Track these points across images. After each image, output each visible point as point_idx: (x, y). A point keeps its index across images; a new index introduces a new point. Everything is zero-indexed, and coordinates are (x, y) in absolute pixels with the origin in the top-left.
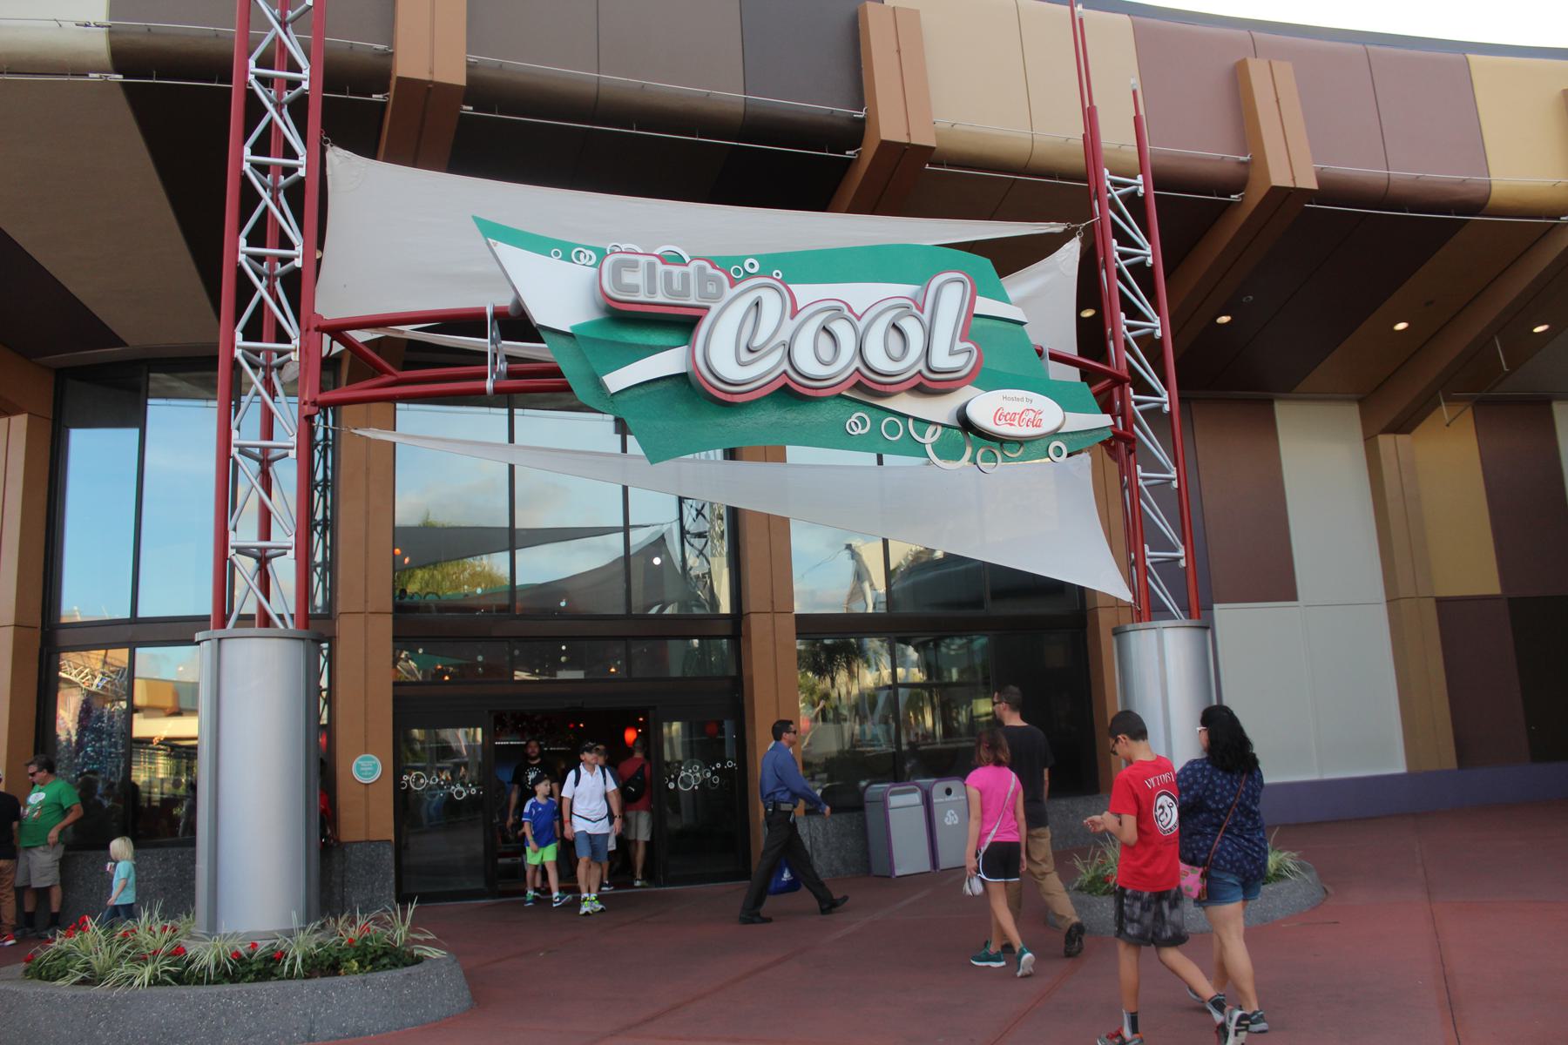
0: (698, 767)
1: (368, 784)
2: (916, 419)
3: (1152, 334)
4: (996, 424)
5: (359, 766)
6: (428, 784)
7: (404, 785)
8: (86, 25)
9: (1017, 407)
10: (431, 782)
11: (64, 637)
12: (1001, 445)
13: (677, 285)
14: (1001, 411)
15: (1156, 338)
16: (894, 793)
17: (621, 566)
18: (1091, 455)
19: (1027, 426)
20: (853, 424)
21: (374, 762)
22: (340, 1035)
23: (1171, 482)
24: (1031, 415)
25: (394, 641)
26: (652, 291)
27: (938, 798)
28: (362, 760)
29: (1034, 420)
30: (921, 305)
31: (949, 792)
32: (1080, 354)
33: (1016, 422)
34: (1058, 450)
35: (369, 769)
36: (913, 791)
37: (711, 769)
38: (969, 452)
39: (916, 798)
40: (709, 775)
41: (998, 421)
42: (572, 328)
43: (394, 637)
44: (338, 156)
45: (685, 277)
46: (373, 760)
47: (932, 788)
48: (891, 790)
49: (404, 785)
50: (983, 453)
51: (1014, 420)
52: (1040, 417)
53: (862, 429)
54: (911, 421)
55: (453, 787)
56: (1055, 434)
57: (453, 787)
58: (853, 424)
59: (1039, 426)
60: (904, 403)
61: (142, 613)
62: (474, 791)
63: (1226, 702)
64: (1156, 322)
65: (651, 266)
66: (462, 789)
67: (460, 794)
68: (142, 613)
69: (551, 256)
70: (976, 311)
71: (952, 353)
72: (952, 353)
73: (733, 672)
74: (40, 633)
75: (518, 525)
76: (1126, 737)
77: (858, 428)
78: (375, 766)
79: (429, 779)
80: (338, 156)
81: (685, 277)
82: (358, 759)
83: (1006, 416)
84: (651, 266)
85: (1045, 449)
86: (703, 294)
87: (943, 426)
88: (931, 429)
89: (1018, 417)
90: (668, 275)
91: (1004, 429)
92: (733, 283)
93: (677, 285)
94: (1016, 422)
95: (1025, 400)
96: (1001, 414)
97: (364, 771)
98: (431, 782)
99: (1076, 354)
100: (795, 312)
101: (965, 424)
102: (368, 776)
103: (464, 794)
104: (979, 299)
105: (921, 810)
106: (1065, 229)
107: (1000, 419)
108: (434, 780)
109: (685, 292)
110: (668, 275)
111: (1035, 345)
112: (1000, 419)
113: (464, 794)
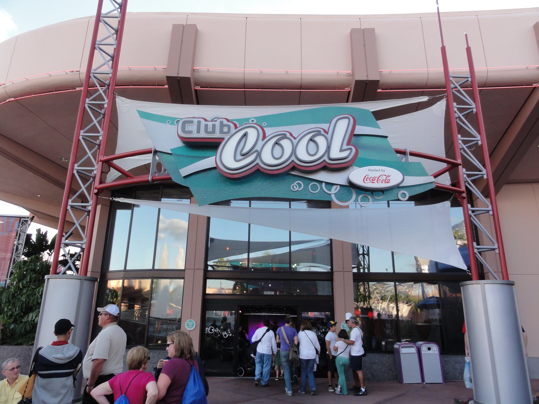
0: (315, 330)
1: (190, 331)
2: (327, 183)
3: (477, 143)
4: (364, 183)
5: (188, 324)
6: (215, 331)
7: (206, 331)
8: (73, 72)
9: (377, 174)
10: (216, 331)
11: (109, 275)
12: (372, 193)
13: (210, 129)
14: (367, 176)
15: (479, 145)
16: (403, 347)
17: (250, 251)
18: (451, 202)
19: (382, 183)
20: (295, 186)
21: (193, 323)
22: (452, 376)
23: (489, 212)
24: (384, 177)
25: (354, 282)
26: (198, 132)
27: (424, 349)
28: (189, 322)
29: (386, 180)
30: (327, 131)
31: (429, 349)
32: (447, 157)
33: (376, 181)
34: (404, 195)
35: (192, 325)
36: (413, 347)
37: (320, 331)
38: (354, 196)
39: (413, 350)
40: (319, 334)
41: (365, 180)
42: (171, 150)
43: (354, 280)
44: (120, 100)
45: (214, 126)
46: (193, 322)
47: (421, 347)
48: (401, 346)
49: (206, 331)
50: (362, 197)
51: (374, 180)
52: (389, 178)
53: (299, 188)
54: (324, 184)
55: (223, 333)
56: (398, 187)
57: (223, 333)
58: (295, 186)
59: (389, 183)
60: (323, 176)
61: (128, 268)
62: (231, 335)
63: (304, 332)
64: (478, 137)
65: (199, 123)
66: (226, 334)
67: (225, 335)
68: (128, 268)
69: (166, 123)
70: (356, 133)
71: (341, 150)
72: (341, 150)
73: (331, 294)
74: (100, 274)
75: (251, 241)
76: (160, 360)
77: (297, 187)
78: (193, 324)
79: (215, 329)
80: (120, 100)
81: (214, 126)
82: (187, 321)
83: (370, 178)
84: (199, 123)
85: (397, 195)
86: (221, 132)
87: (341, 185)
88: (335, 187)
89: (376, 179)
90: (206, 126)
91: (369, 185)
92: (236, 127)
93: (210, 129)
94: (376, 181)
95: (380, 170)
96: (367, 178)
97: (189, 326)
98: (216, 331)
99: (445, 157)
100: (264, 137)
101: (352, 185)
102: (191, 328)
103: (227, 336)
104: (357, 127)
105: (416, 356)
106: (428, 99)
107: (366, 180)
108: (217, 330)
109: (213, 132)
110: (206, 126)
111: (394, 149)
112: (366, 180)
113: (227, 336)
